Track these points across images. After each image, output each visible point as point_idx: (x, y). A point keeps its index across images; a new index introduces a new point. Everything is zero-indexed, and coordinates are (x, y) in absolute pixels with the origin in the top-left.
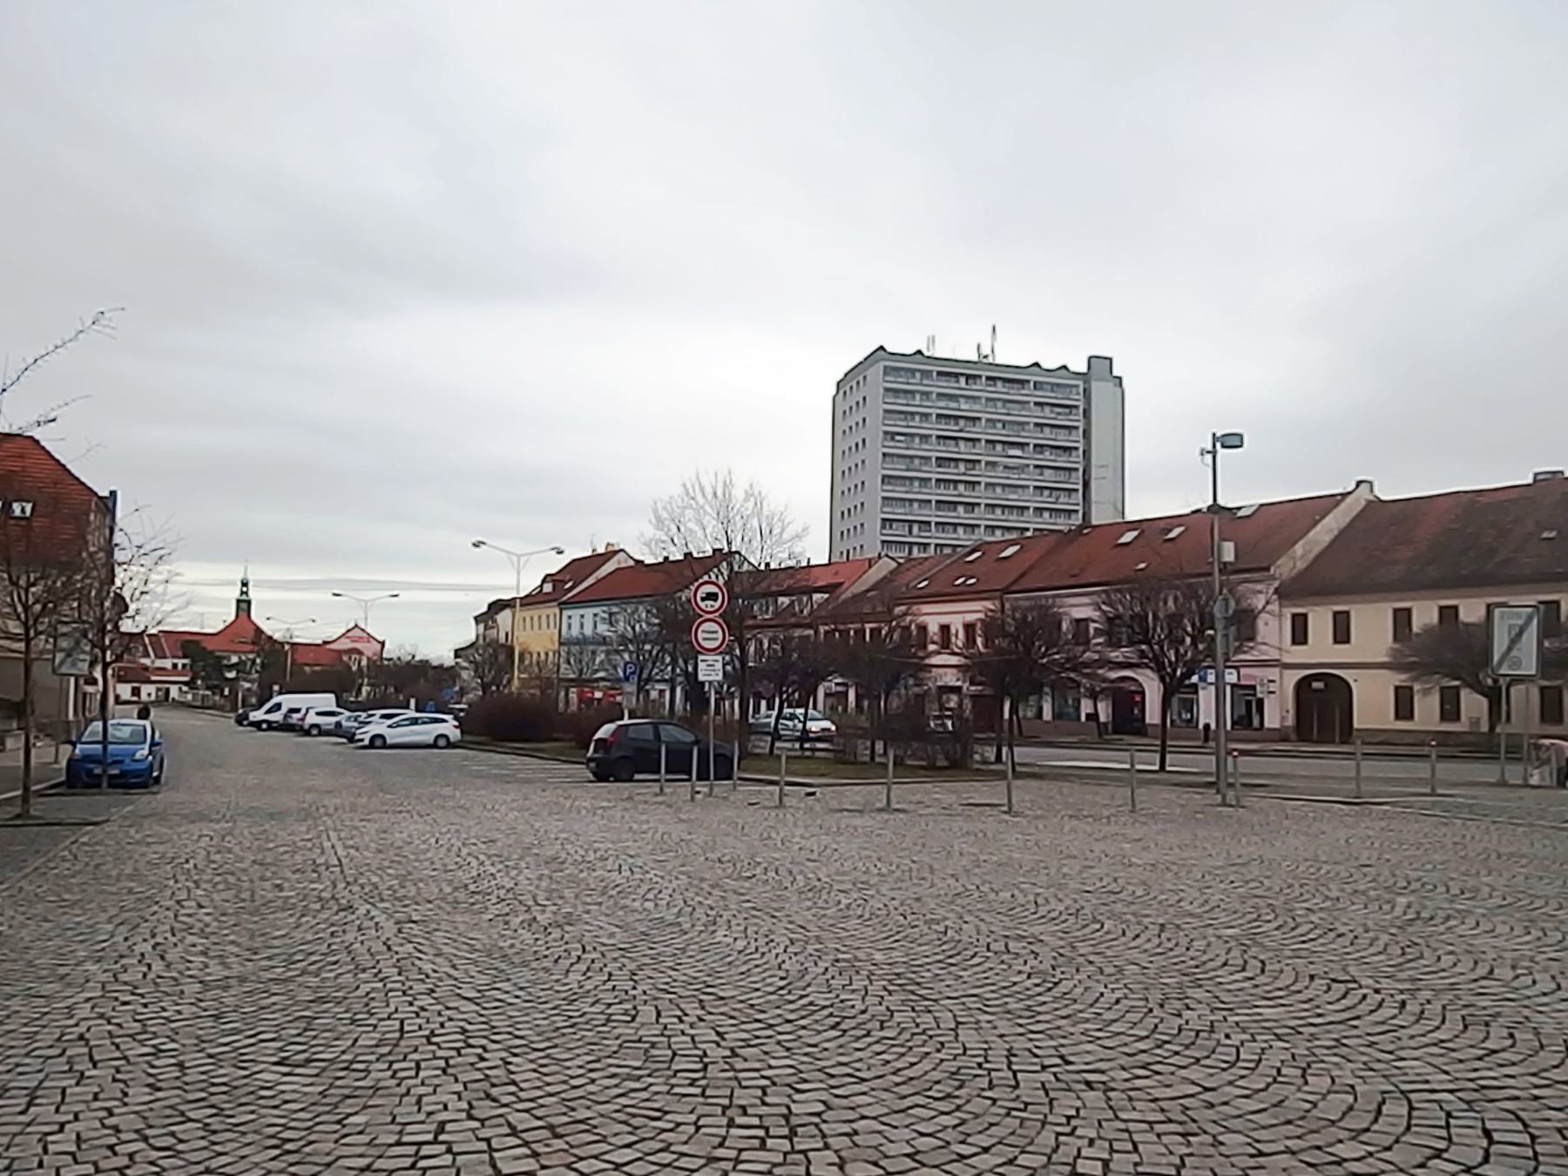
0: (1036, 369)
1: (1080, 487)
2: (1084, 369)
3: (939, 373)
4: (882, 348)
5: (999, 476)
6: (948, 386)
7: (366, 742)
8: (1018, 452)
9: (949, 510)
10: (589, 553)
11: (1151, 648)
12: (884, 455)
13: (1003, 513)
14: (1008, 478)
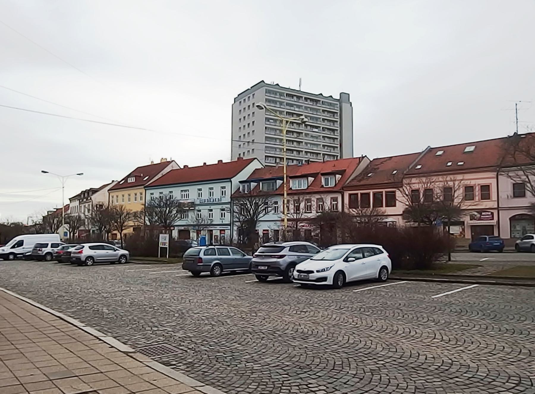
0: (321, 96)
1: (339, 146)
2: (339, 98)
3: (287, 94)
4: (263, 81)
5: (309, 140)
6: (288, 100)
7: (330, 282)
8: (316, 130)
9: (290, 153)
10: (150, 164)
11: (118, 224)
12: (266, 128)
13: (334, 150)
14: (313, 141)
